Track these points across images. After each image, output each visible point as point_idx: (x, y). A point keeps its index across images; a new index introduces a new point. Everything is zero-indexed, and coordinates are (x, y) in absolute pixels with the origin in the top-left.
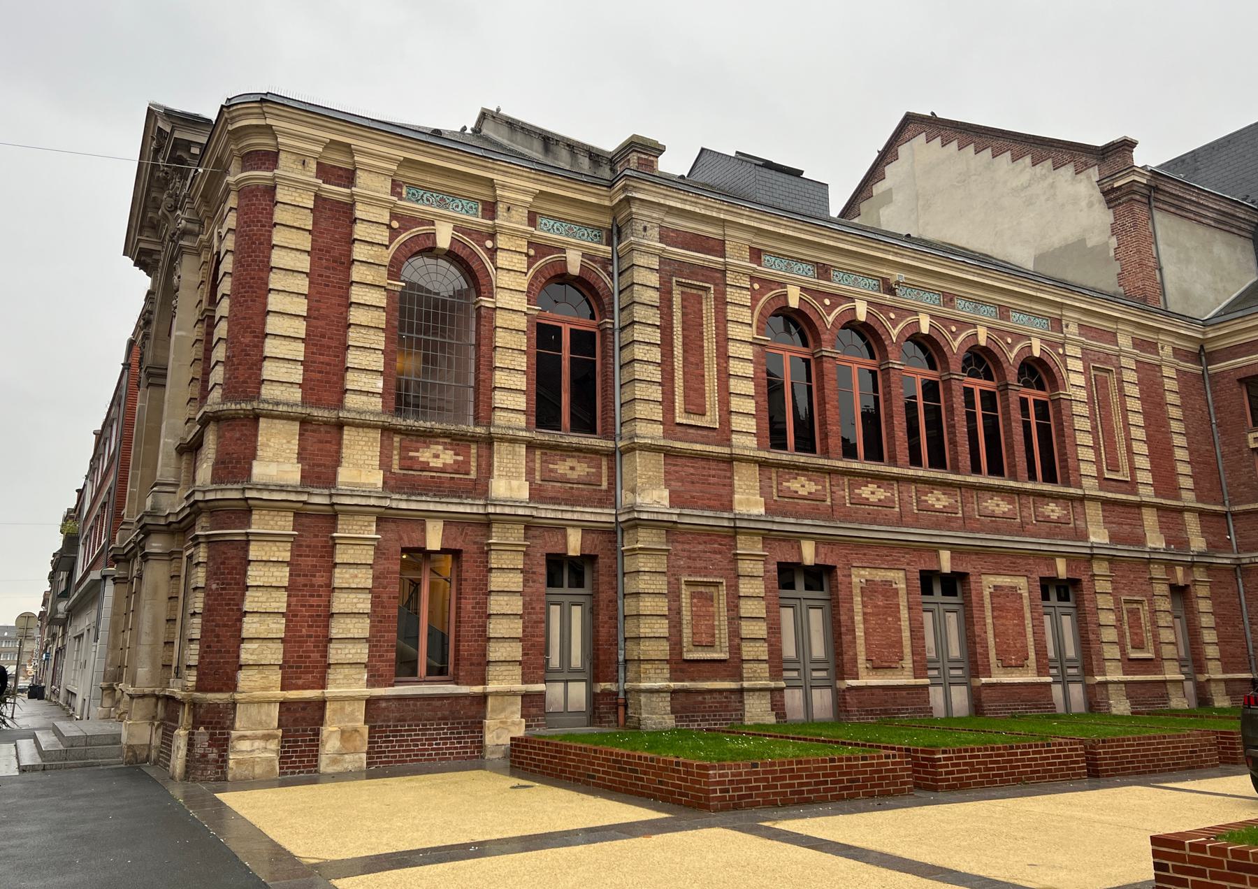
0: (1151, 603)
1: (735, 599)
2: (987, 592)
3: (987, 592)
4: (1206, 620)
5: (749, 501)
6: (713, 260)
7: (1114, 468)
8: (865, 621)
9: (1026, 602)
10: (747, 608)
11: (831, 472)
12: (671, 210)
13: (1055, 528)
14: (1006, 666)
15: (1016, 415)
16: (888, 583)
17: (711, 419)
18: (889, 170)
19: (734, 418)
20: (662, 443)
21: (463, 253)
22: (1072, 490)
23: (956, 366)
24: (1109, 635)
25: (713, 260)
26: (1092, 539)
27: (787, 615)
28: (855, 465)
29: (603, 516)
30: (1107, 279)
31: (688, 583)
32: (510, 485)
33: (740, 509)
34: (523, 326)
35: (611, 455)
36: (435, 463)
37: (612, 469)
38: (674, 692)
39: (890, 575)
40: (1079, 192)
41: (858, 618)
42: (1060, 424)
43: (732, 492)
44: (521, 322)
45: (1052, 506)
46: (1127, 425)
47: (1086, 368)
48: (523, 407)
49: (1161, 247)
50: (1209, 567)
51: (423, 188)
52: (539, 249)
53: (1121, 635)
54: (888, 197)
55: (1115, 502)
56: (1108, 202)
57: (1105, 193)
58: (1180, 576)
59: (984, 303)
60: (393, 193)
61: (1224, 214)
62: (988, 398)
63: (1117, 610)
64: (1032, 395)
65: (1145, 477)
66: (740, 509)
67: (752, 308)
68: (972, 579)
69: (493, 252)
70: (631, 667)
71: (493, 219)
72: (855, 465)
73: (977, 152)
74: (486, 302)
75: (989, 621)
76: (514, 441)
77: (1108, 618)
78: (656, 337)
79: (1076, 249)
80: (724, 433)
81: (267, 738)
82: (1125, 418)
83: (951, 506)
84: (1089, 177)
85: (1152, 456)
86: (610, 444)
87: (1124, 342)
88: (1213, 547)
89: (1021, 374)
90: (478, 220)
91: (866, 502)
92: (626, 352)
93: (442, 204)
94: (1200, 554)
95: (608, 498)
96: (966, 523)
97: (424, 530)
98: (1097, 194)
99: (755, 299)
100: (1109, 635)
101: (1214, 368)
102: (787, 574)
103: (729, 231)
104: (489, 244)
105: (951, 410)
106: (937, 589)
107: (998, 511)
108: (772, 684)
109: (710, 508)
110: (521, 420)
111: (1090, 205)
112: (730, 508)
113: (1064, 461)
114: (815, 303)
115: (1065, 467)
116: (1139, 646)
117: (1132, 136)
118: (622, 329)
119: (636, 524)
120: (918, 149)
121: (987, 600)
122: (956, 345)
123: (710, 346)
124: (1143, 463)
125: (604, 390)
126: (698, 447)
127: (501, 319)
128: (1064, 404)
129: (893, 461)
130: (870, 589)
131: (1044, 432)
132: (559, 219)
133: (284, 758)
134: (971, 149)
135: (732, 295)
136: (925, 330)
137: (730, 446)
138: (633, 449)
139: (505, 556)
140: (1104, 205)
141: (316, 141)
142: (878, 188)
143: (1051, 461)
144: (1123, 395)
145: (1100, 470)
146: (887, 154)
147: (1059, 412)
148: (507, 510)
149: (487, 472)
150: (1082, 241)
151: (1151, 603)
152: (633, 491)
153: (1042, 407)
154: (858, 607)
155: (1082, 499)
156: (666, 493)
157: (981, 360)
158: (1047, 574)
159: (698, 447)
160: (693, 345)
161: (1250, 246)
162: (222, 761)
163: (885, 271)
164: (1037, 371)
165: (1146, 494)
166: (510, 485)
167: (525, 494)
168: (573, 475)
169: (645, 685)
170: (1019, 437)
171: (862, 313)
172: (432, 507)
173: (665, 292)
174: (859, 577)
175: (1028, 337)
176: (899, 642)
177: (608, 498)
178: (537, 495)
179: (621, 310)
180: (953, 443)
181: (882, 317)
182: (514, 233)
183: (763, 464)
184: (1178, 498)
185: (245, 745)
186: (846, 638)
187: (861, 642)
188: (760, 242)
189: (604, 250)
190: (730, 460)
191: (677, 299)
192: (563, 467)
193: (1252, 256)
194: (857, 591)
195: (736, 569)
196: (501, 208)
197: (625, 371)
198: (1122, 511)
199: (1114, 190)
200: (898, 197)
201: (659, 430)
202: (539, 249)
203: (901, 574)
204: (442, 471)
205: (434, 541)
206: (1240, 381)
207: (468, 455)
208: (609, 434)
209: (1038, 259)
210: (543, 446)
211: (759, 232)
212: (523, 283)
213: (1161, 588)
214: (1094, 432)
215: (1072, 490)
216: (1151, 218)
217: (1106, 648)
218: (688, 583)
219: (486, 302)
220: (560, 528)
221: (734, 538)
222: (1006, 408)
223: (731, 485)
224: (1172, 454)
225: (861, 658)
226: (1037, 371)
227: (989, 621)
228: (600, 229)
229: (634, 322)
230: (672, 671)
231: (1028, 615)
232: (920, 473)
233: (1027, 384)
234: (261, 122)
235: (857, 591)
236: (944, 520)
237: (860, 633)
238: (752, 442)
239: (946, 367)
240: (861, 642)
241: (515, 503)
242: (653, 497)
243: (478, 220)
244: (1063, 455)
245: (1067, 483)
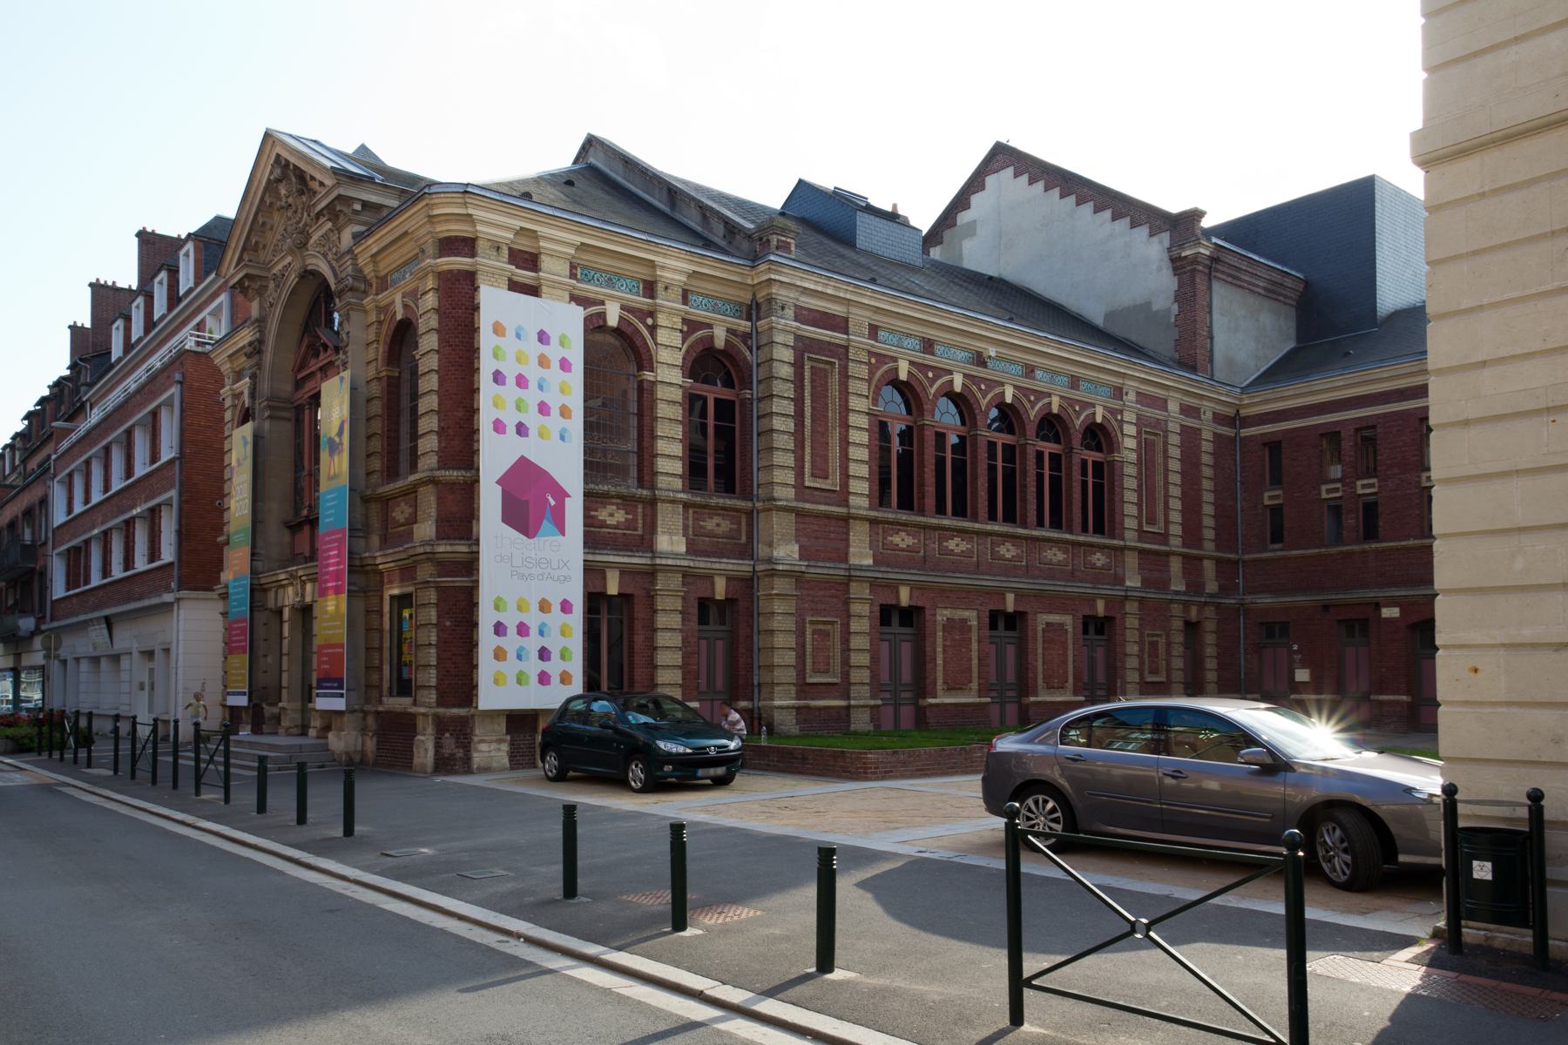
0: (1168, 636)
1: (847, 634)
2: (1040, 628)
3: (1040, 628)
4: (1210, 651)
5: (861, 554)
6: (838, 337)
7: (1152, 520)
8: (944, 651)
9: (1070, 636)
10: (855, 642)
11: (926, 527)
12: (805, 291)
13: (1098, 576)
14: (1050, 687)
15: (1077, 476)
16: (964, 621)
17: (833, 483)
18: (976, 200)
19: (851, 481)
20: (795, 504)
21: (629, 331)
22: (1116, 542)
23: (1031, 430)
24: (1132, 663)
25: (838, 337)
26: (1128, 583)
27: (885, 646)
28: (946, 522)
29: (742, 567)
30: (1163, 342)
31: (812, 622)
32: (670, 542)
33: (853, 561)
34: (679, 398)
35: (750, 514)
36: (611, 521)
37: (750, 525)
38: (798, 709)
39: (966, 614)
40: (1153, 249)
41: (939, 649)
42: (1112, 483)
43: (848, 546)
44: (677, 395)
45: (1098, 555)
46: (1166, 483)
47: (1139, 432)
48: (680, 471)
49: (1216, 316)
50: (1218, 606)
51: (594, 269)
52: (691, 325)
53: (1142, 663)
54: (971, 228)
55: (1150, 552)
56: (1175, 269)
57: (1172, 260)
58: (1193, 614)
59: (1057, 373)
60: (573, 276)
61: (1274, 283)
62: (1055, 458)
63: (1141, 642)
64: (1092, 456)
65: (1176, 530)
66: (853, 561)
67: (869, 381)
68: (1030, 617)
69: (653, 329)
70: (764, 690)
71: (652, 297)
72: (946, 522)
73: (1062, 197)
74: (648, 376)
75: (1040, 651)
76: (673, 501)
77: (1132, 649)
78: (791, 409)
79: (1143, 310)
80: (843, 495)
81: (500, 741)
82: (1166, 477)
83: (1018, 556)
84: (1161, 242)
85: (1184, 512)
86: (750, 504)
87: (1173, 407)
88: (1224, 590)
89: (1084, 438)
90: (642, 301)
91: (952, 552)
92: (764, 421)
93: (610, 283)
94: (1211, 596)
95: (746, 551)
96: (1028, 571)
97: (604, 578)
98: (1166, 257)
99: (872, 373)
100: (1132, 663)
101: (1245, 432)
102: (886, 614)
103: (853, 310)
104: (650, 321)
105: (1024, 473)
106: (895, 620)
107: (1055, 559)
108: (872, 702)
109: (830, 560)
110: (678, 483)
111: (1159, 269)
112: (845, 559)
113: (1112, 515)
114: (920, 376)
115: (1112, 521)
116: (1154, 671)
117: (1202, 207)
118: (760, 400)
119: (773, 573)
120: (1003, 182)
121: (1040, 634)
122: (1033, 413)
123: (833, 415)
124: (1176, 517)
125: (743, 454)
126: (822, 508)
127: (661, 392)
128: (1117, 465)
129: (975, 519)
130: (950, 625)
131: (1098, 489)
132: (707, 296)
133: (512, 756)
134: (1056, 192)
135: (853, 369)
136: (1009, 400)
137: (847, 506)
138: (770, 510)
139: (668, 600)
140: (1170, 272)
141: (507, 228)
142: (963, 218)
143: (1102, 519)
144: (1166, 457)
145: (1140, 524)
146: (975, 183)
147: (1112, 473)
148: (670, 562)
149: (651, 528)
150: (1148, 304)
151: (1168, 636)
152: (770, 545)
153: (1098, 466)
154: (939, 641)
155: (1123, 549)
156: (796, 548)
157: (1052, 425)
158: (1088, 612)
159: (822, 508)
160: (820, 415)
161: (1292, 312)
162: (467, 760)
163: (979, 345)
164: (1099, 436)
165: (1175, 543)
166: (670, 542)
167: (682, 549)
168: (719, 531)
169: (777, 703)
170: (1077, 496)
171: (958, 383)
172: (611, 559)
173: (798, 365)
174: (943, 615)
175: (1093, 406)
176: (969, 669)
177: (746, 551)
178: (692, 550)
179: (759, 382)
180: (1024, 500)
181: (974, 388)
182: (672, 312)
183: (873, 522)
184: (1200, 547)
185: (484, 747)
186: (929, 666)
187: (940, 669)
188: (879, 319)
189: (744, 326)
190: (846, 520)
191: (807, 374)
192: (710, 524)
193: (1293, 324)
194: (939, 628)
195: (848, 610)
196: (660, 286)
197: (763, 438)
198: (1153, 561)
199: (1180, 258)
200: (982, 231)
201: (791, 493)
202: (691, 325)
203: (974, 614)
204: (616, 527)
205: (613, 589)
206: (1264, 444)
207: (635, 515)
208: (747, 495)
209: (1109, 316)
210: (694, 505)
211: (877, 310)
212: (678, 358)
213: (1178, 624)
214: (1139, 491)
215: (1116, 542)
216: (1210, 288)
217: (1128, 673)
218: (812, 622)
219: (648, 376)
220: (709, 578)
221: (847, 585)
222: (1070, 469)
223: (847, 540)
224: (1200, 506)
225: (940, 681)
226: (1099, 436)
227: (1040, 651)
228: (741, 304)
229: (772, 396)
230: (798, 692)
231: (1070, 647)
232: (996, 528)
233: (1088, 448)
234: (462, 211)
235: (939, 628)
236: (1009, 569)
237: (940, 661)
238: (865, 502)
239: (1024, 434)
240: (940, 669)
241: (676, 556)
242: (787, 552)
243: (642, 301)
244: (1112, 510)
245: (1113, 536)
